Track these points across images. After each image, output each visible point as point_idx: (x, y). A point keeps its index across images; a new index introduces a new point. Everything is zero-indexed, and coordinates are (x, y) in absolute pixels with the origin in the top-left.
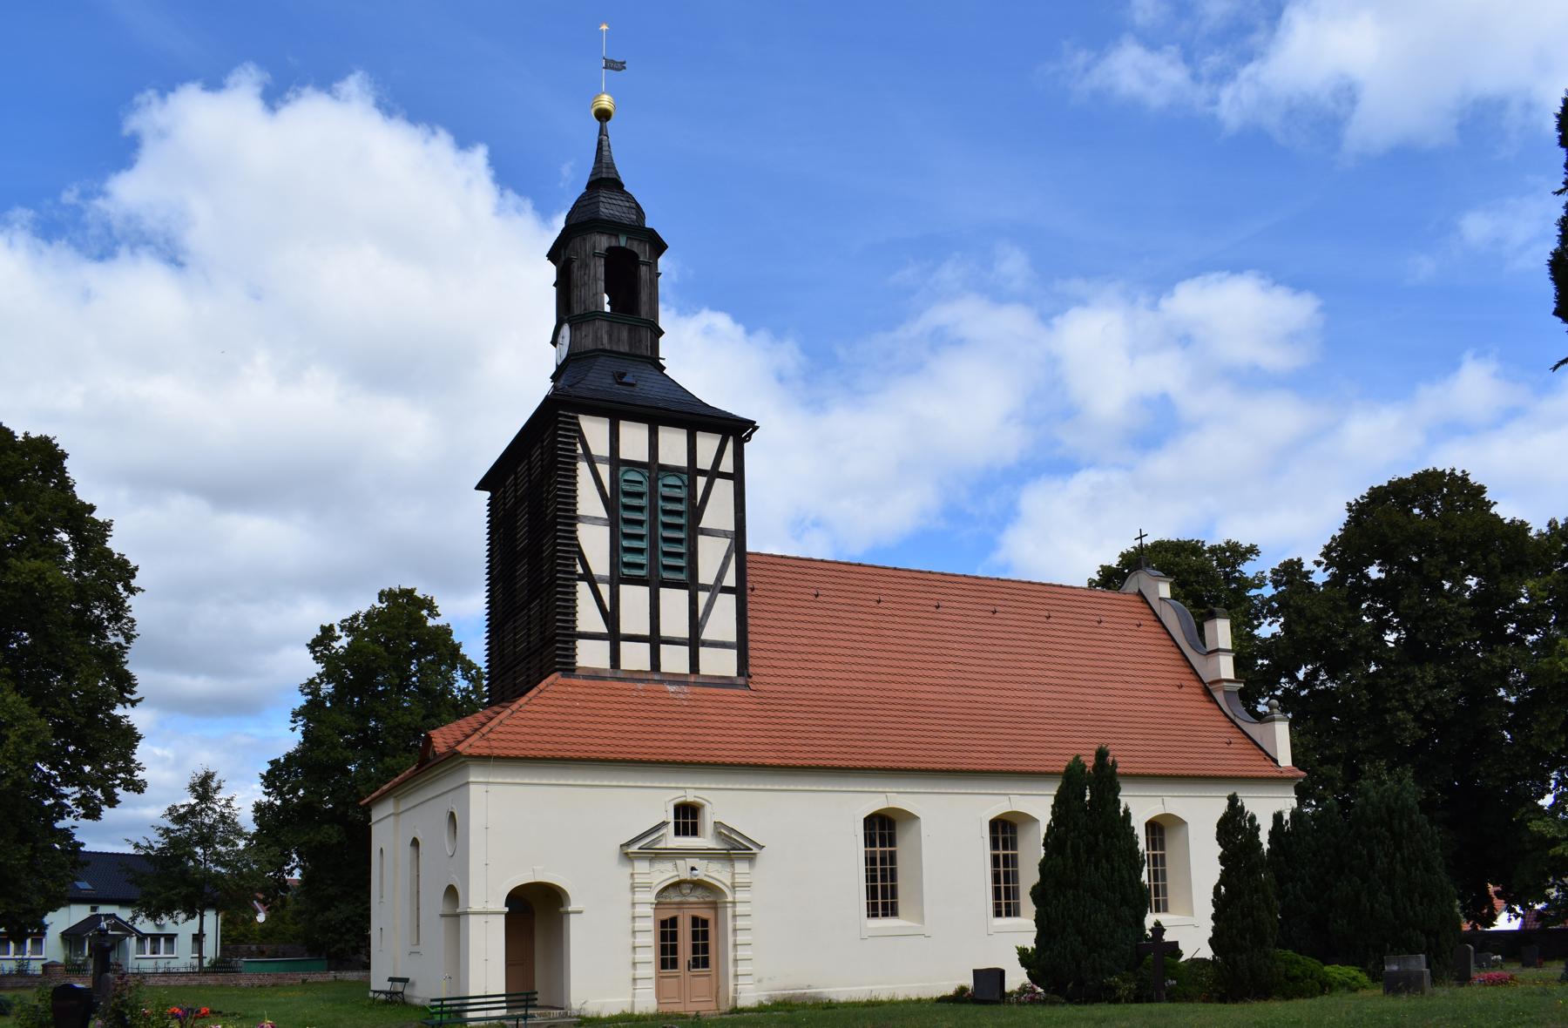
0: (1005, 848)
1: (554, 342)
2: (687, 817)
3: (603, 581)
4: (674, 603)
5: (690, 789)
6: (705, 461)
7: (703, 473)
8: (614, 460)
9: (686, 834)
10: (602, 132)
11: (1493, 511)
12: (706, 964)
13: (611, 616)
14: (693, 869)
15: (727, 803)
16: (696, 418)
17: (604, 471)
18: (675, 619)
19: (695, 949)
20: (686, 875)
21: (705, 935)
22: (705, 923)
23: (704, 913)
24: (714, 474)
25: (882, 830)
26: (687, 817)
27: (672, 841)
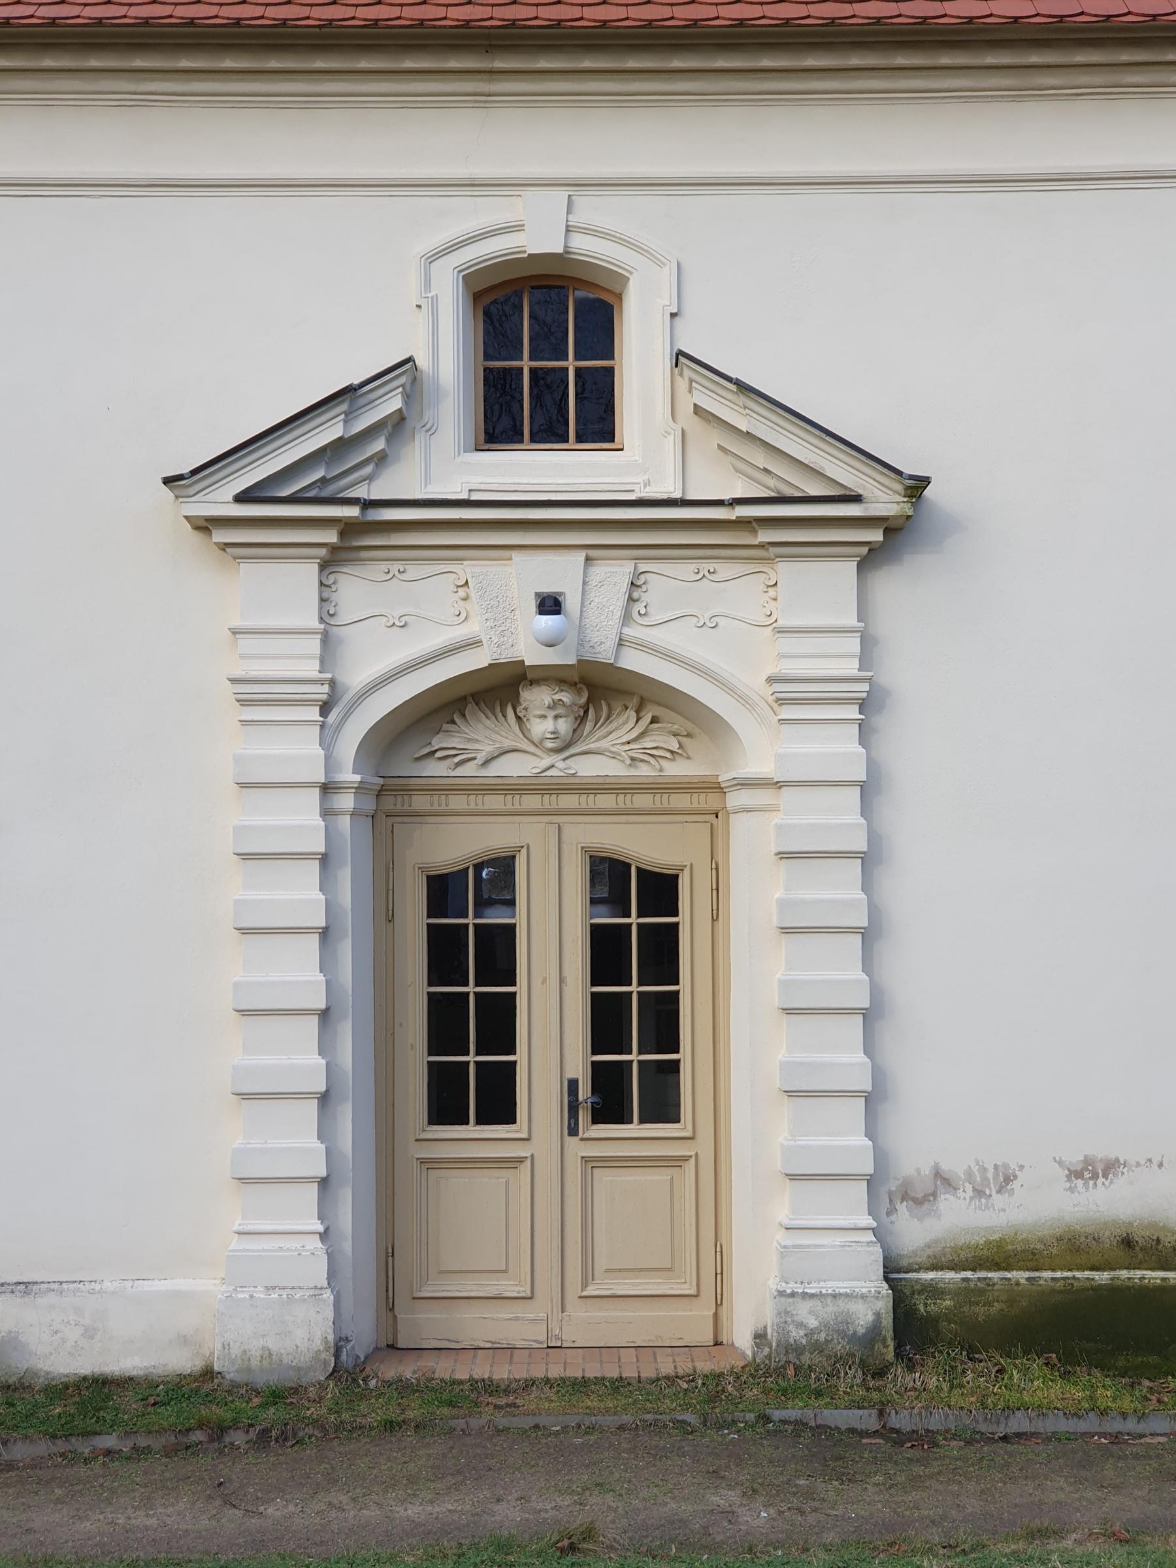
2: (543, 346)
5: (543, 169)
9: (550, 432)
11: (742, 1339)
12: (663, 1105)
14: (550, 605)
15: (777, 248)
19: (607, 1025)
20: (528, 640)
21: (663, 954)
22: (661, 890)
23: (646, 846)
26: (543, 346)
27: (448, 463)
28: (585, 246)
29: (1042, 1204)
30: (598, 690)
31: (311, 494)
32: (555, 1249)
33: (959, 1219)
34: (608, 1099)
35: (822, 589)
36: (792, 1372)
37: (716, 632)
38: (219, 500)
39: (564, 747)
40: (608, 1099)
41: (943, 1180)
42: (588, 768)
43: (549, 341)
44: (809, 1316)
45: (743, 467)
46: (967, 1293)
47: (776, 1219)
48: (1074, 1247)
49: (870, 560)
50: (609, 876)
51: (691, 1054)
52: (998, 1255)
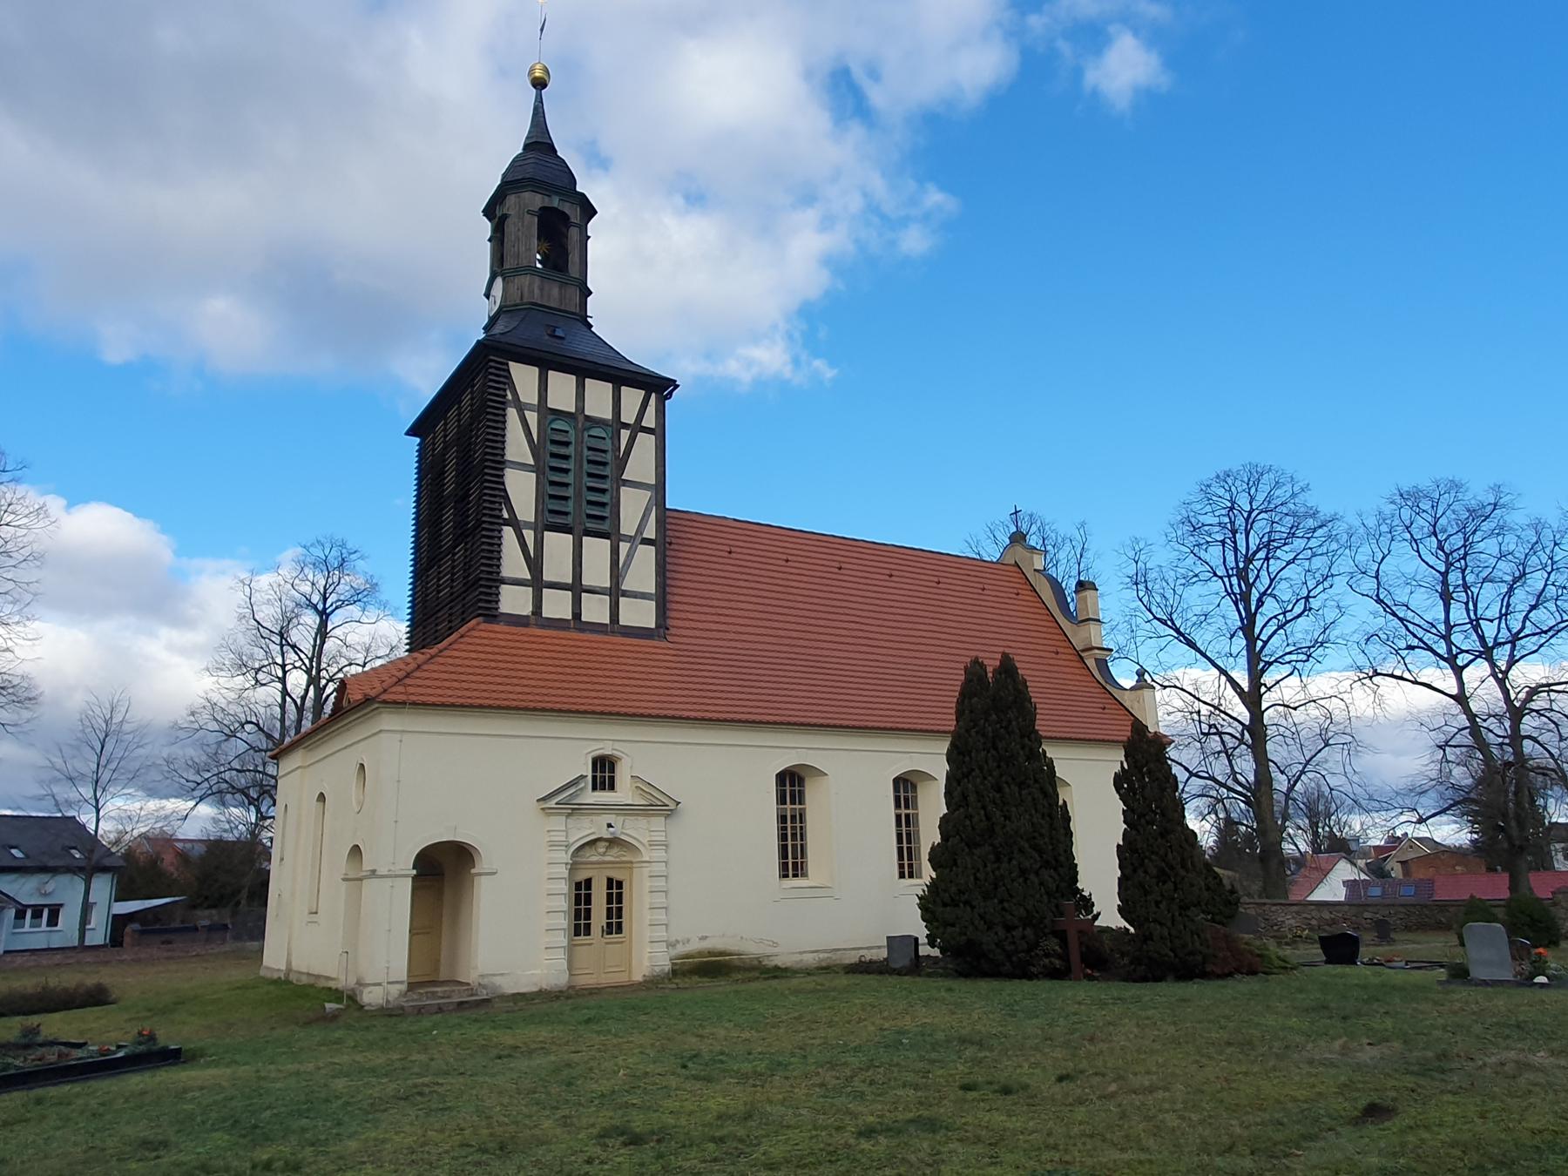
1: (487, 295)
2: (604, 771)
3: (528, 525)
4: (597, 551)
6: (628, 416)
7: (626, 426)
8: (542, 407)
12: (619, 929)
13: (535, 563)
15: (647, 756)
16: (621, 374)
17: (532, 418)
18: (597, 571)
20: (606, 833)
22: (620, 884)
23: (617, 875)
24: (638, 428)
25: (791, 783)
26: (604, 771)
29: (695, 946)
30: (614, 842)
31: (562, 802)
33: (681, 949)
35: (658, 823)
37: (634, 830)
38: (552, 803)
44: (657, 969)
47: (648, 949)
48: (700, 954)
49: (667, 816)
51: (624, 920)
52: (687, 956)
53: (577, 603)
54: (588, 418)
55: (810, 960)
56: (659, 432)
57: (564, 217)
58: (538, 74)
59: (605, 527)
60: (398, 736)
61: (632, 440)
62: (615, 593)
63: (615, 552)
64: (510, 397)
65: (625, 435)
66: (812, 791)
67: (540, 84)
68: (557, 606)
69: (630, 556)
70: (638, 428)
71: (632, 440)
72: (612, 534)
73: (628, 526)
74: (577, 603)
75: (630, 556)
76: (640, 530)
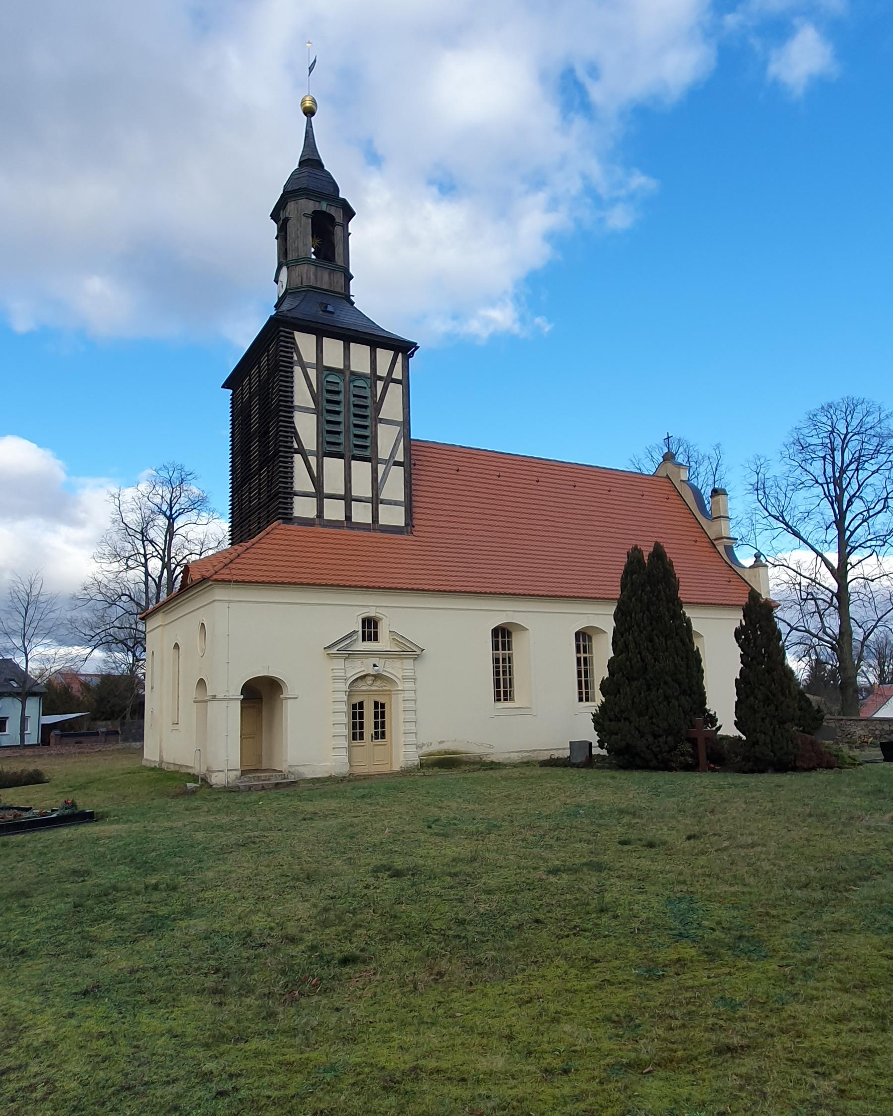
0: (504, 649)
3: (312, 453)
4: (361, 471)
6: (382, 371)
7: (380, 378)
9: (370, 640)
10: (309, 125)
12: (383, 735)
13: (317, 481)
15: (400, 617)
16: (378, 340)
17: (312, 373)
18: (362, 486)
22: (383, 706)
23: (381, 700)
24: (389, 380)
25: (502, 636)
28: (378, 615)
31: (340, 649)
32: (375, 759)
34: (376, 736)
35: (409, 663)
36: (406, 772)
37: (393, 669)
38: (334, 650)
39: (371, 685)
40: (376, 736)
41: (424, 745)
42: (374, 688)
43: (369, 628)
45: (399, 647)
46: (426, 760)
47: (403, 749)
48: (439, 753)
49: (415, 659)
50: (376, 704)
53: (348, 509)
54: (353, 373)
55: (515, 757)
56: (405, 382)
57: (331, 218)
58: (308, 104)
59: (367, 453)
60: (227, 604)
61: (385, 389)
62: (375, 501)
63: (375, 471)
64: (295, 358)
65: (380, 385)
66: (517, 641)
67: (309, 113)
68: (334, 511)
69: (386, 474)
70: (389, 380)
71: (385, 389)
72: (372, 459)
73: (384, 452)
74: (348, 509)
75: (386, 474)
76: (392, 455)
